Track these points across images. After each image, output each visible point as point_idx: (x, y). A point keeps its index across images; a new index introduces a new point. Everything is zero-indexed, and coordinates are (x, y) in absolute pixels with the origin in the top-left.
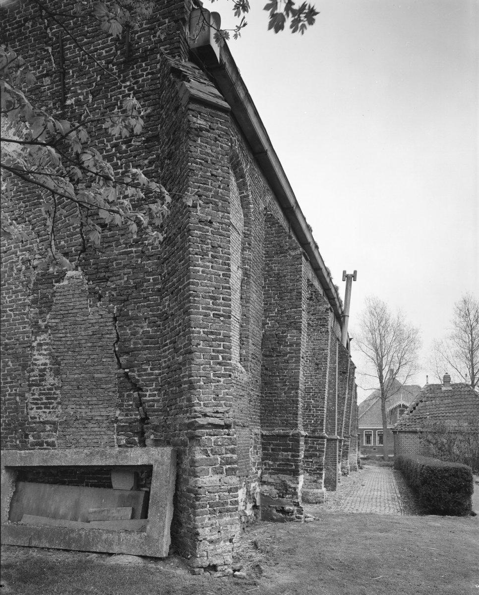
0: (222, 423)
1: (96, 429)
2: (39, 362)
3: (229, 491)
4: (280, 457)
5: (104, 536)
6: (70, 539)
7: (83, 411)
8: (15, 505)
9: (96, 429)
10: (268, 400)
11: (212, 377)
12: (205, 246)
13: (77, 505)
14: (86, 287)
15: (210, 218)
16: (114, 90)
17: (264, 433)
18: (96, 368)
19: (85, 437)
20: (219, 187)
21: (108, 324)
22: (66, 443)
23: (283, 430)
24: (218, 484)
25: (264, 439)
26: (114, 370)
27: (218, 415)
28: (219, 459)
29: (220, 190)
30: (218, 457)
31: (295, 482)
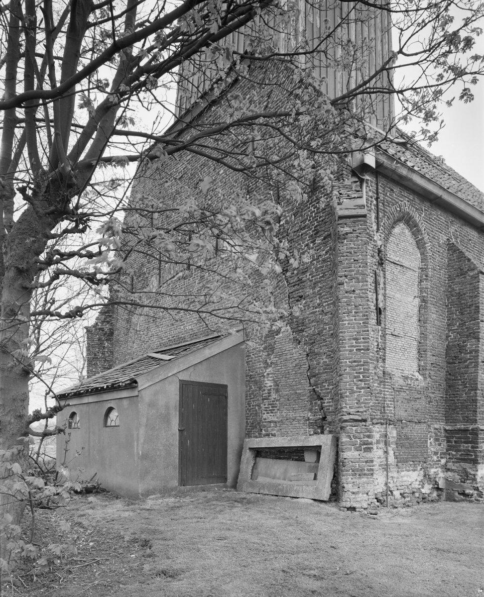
0: (360, 418)
1: (297, 425)
2: (268, 385)
3: (366, 462)
4: (462, 448)
5: (295, 488)
6: (279, 489)
7: (291, 414)
8: (254, 471)
9: (297, 425)
10: (451, 400)
11: (355, 389)
12: (349, 308)
13: (286, 471)
14: (292, 337)
15: (353, 289)
16: (306, 210)
17: (447, 428)
18: (298, 387)
19: (291, 430)
20: (360, 267)
21: (304, 359)
22: (281, 434)
23: (464, 425)
24: (358, 457)
25: (448, 433)
26: (308, 388)
27: (358, 413)
28: (359, 441)
29: (360, 269)
30: (358, 440)
31: (474, 469)
